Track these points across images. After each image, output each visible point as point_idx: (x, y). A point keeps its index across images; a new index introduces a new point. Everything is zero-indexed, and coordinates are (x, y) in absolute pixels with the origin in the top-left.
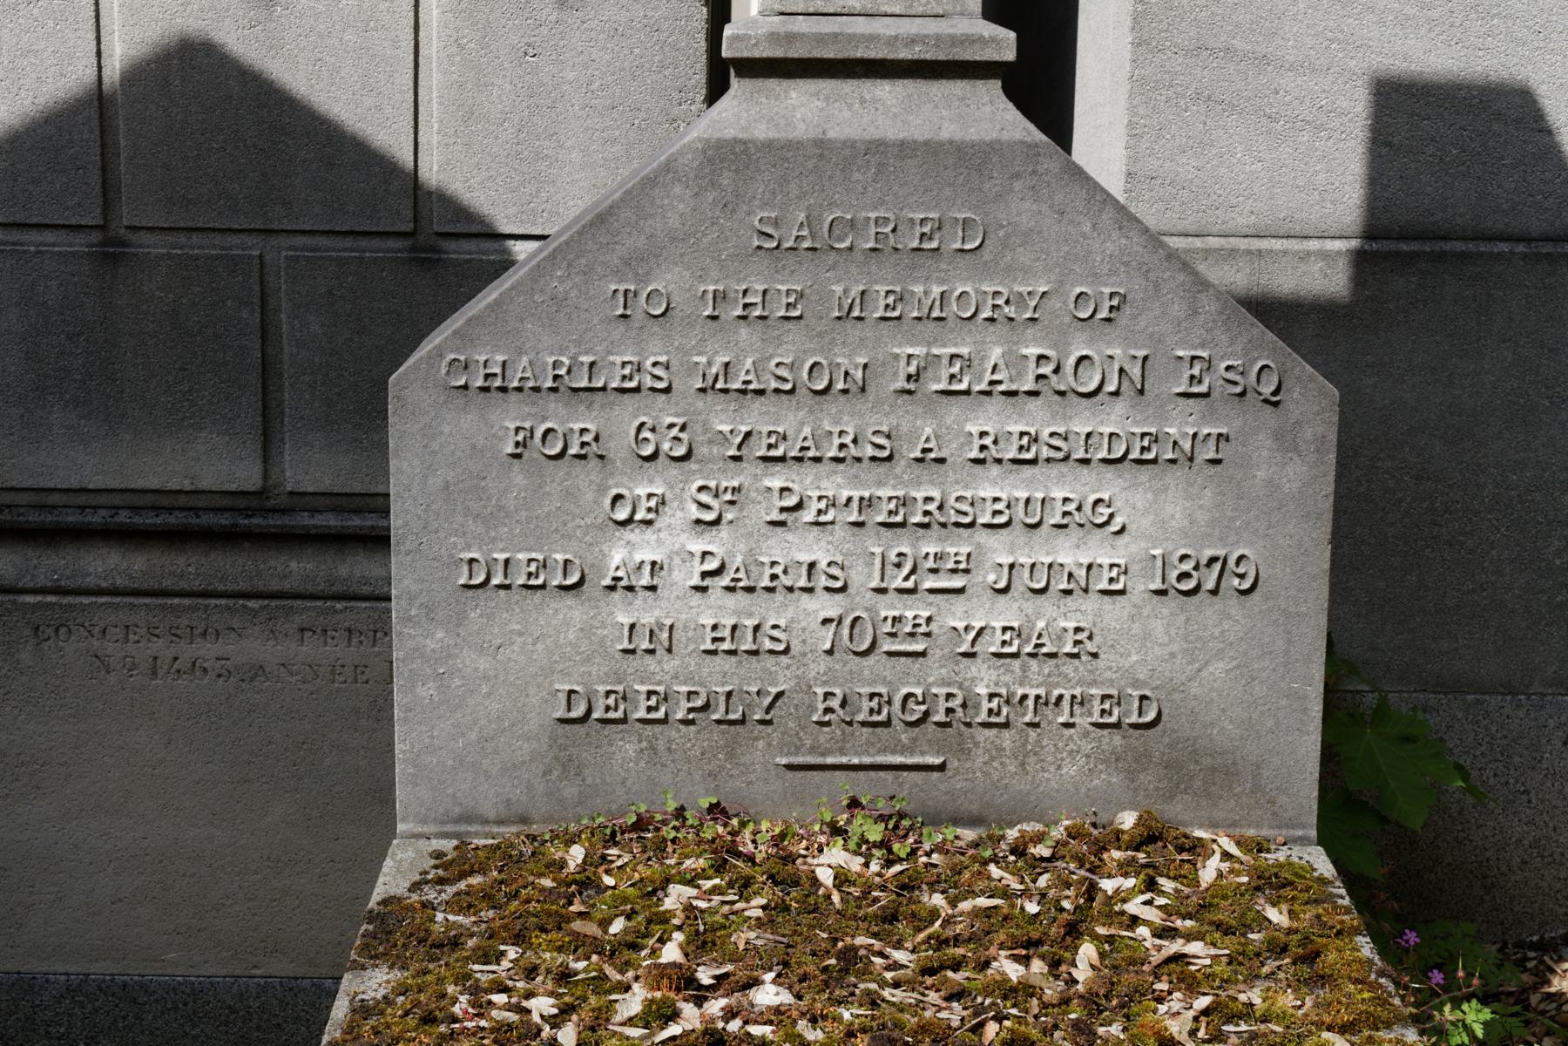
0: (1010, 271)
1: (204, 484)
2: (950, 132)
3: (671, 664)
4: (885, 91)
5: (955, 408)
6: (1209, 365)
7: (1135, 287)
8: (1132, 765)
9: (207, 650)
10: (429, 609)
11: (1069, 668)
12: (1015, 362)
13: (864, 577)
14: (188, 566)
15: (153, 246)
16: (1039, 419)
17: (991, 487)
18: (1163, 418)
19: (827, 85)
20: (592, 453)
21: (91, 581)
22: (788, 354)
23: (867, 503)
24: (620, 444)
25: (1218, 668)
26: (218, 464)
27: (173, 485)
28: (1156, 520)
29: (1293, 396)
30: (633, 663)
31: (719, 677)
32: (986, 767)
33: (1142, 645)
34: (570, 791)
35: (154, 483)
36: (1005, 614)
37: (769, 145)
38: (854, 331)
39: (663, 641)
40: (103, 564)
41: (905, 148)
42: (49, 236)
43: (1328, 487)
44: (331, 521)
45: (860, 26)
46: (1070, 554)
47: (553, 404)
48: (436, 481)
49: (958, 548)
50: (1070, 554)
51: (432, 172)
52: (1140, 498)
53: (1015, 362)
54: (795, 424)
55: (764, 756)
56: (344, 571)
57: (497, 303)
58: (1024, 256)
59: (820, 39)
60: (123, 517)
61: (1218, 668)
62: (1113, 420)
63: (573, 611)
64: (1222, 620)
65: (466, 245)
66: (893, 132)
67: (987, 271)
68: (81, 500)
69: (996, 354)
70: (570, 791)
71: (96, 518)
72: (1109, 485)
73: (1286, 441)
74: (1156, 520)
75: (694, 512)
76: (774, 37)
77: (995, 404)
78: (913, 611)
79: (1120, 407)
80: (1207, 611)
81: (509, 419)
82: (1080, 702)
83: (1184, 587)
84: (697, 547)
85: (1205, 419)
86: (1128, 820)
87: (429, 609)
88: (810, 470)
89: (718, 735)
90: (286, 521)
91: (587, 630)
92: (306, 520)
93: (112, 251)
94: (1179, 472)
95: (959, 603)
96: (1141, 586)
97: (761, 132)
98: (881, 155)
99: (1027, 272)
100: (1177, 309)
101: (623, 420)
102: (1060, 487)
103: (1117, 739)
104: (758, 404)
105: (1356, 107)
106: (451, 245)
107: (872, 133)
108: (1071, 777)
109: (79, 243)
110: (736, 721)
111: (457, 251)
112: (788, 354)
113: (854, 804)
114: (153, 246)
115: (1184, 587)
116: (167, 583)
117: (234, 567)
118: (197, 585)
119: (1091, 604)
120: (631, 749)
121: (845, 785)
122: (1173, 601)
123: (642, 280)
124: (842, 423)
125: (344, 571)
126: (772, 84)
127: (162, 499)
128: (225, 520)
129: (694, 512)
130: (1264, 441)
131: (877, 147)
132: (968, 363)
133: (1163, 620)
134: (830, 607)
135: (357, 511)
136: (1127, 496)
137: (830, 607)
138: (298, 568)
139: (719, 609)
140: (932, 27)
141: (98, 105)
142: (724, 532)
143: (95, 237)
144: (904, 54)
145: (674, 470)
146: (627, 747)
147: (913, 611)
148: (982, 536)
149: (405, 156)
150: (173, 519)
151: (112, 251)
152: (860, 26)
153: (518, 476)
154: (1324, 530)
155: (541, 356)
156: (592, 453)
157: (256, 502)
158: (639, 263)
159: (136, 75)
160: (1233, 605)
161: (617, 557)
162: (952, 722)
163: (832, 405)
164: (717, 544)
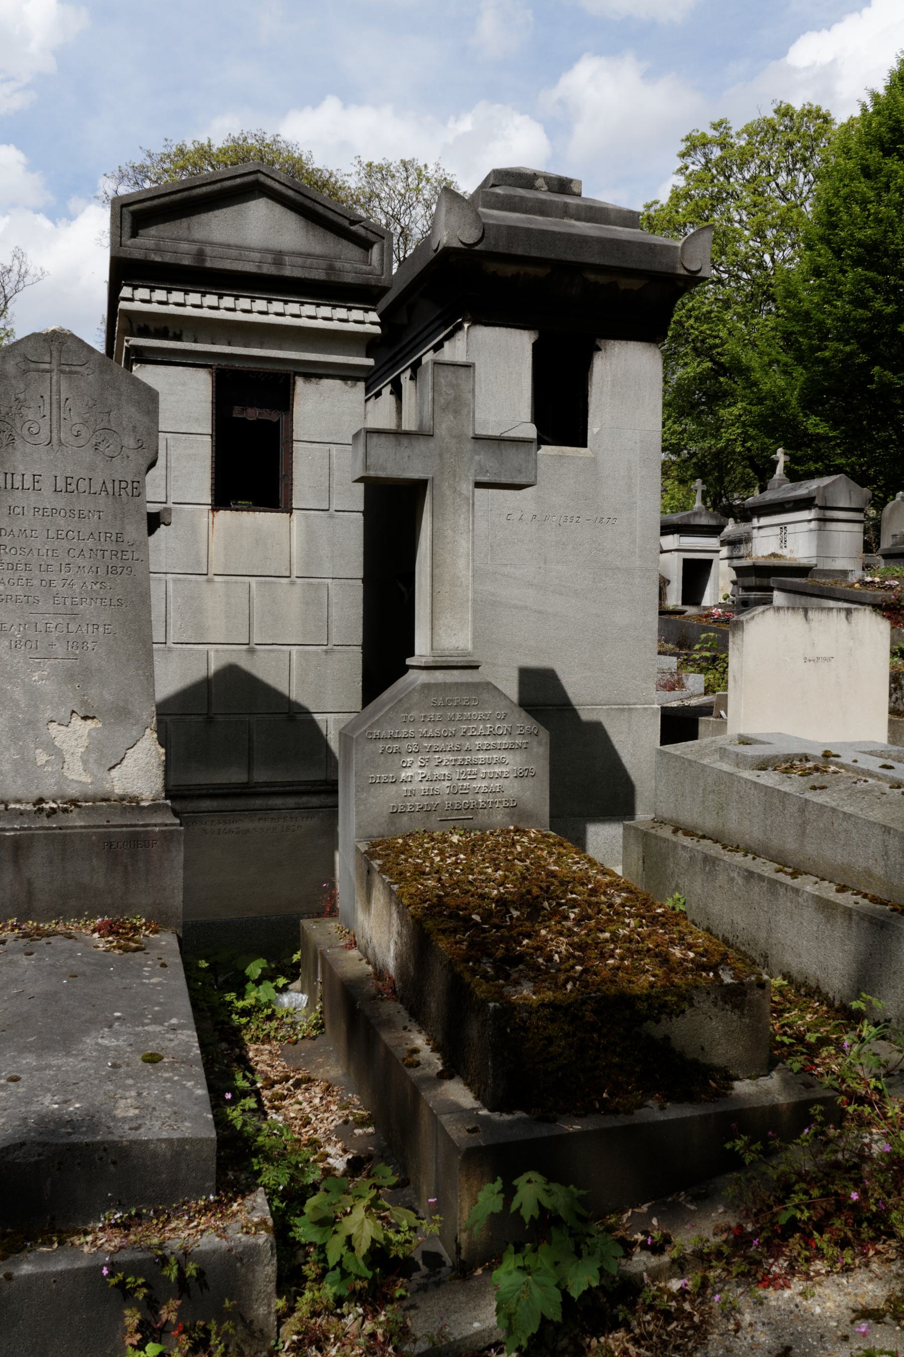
0: (484, 709)
1: (233, 781)
2: (470, 680)
3: (415, 798)
4: (455, 672)
5: (473, 739)
6: (524, 728)
7: (508, 711)
8: (511, 815)
9: (233, 826)
10: (363, 789)
11: (498, 795)
12: (485, 728)
13: (455, 777)
14: (229, 804)
15: (220, 718)
16: (490, 741)
17: (481, 756)
18: (515, 739)
19: (444, 671)
20: (398, 752)
21: (203, 809)
22: (439, 729)
23: (456, 760)
24: (403, 751)
25: (528, 793)
26: (236, 776)
27: (224, 782)
28: (513, 762)
29: (541, 733)
30: (406, 799)
31: (425, 801)
32: (481, 818)
33: (513, 789)
34: (393, 829)
35: (219, 782)
36: (484, 784)
37: (434, 684)
38: (453, 723)
39: (413, 793)
40: (206, 804)
41: (462, 684)
42: (193, 717)
43: (548, 753)
44: (267, 789)
45: (449, 659)
46: (497, 769)
47: (390, 741)
48: (364, 759)
49: (475, 770)
50: (497, 769)
51: (294, 697)
52: (511, 757)
53: (485, 728)
54: (440, 744)
55: (435, 818)
56: (270, 802)
57: (378, 720)
58: (487, 706)
59: (443, 662)
60: (211, 791)
61: (528, 793)
62: (505, 740)
63: (394, 788)
64: (529, 782)
65: (301, 715)
66: (459, 681)
67: (479, 709)
68: (198, 787)
69: (481, 727)
70: (393, 829)
71: (204, 792)
72: (504, 754)
73: (540, 743)
74: (513, 762)
75: (420, 764)
76: (433, 662)
77: (481, 738)
78: (466, 784)
79: (506, 737)
80: (526, 780)
81: (380, 745)
82: (501, 802)
83: (520, 776)
84: (420, 771)
85: (524, 739)
86: (512, 828)
87: (363, 789)
88: (444, 754)
89: (425, 814)
90: (252, 790)
91: (396, 792)
92: (259, 789)
93: (209, 720)
94: (518, 751)
95: (475, 782)
96: (512, 776)
97: (433, 681)
98: (458, 686)
99: (487, 709)
100: (517, 716)
101: (405, 744)
102: (495, 755)
103: (508, 810)
104: (433, 740)
105: (515, 674)
106: (298, 715)
107: (455, 681)
108: (499, 818)
109: (200, 718)
110: (428, 811)
111: (300, 717)
112: (439, 729)
113: (454, 828)
114: (220, 718)
115: (520, 776)
116: (223, 809)
117: (241, 803)
118: (231, 808)
119: (502, 780)
120: (406, 818)
121: (452, 823)
122: (519, 779)
123: (408, 713)
124: (451, 743)
125: (270, 802)
126: (432, 671)
127: (221, 786)
128: (239, 790)
129: (420, 764)
130: (535, 743)
131: (456, 684)
132: (476, 729)
133: (516, 783)
134: (447, 784)
135: (273, 787)
136: (507, 756)
137: (447, 784)
138: (258, 802)
139: (424, 786)
140: (464, 659)
141: (207, 683)
142: (426, 768)
143: (205, 716)
144: (459, 664)
145: (415, 755)
146: (405, 818)
147: (466, 784)
148: (480, 767)
149: (286, 692)
150: (225, 791)
151: (209, 720)
152: (449, 659)
153: (382, 758)
154: (548, 762)
155: (388, 731)
156: (398, 752)
157: (245, 785)
158: (408, 710)
159: (218, 674)
160: (530, 779)
161: (403, 775)
162: (474, 809)
163: (448, 739)
164: (424, 771)
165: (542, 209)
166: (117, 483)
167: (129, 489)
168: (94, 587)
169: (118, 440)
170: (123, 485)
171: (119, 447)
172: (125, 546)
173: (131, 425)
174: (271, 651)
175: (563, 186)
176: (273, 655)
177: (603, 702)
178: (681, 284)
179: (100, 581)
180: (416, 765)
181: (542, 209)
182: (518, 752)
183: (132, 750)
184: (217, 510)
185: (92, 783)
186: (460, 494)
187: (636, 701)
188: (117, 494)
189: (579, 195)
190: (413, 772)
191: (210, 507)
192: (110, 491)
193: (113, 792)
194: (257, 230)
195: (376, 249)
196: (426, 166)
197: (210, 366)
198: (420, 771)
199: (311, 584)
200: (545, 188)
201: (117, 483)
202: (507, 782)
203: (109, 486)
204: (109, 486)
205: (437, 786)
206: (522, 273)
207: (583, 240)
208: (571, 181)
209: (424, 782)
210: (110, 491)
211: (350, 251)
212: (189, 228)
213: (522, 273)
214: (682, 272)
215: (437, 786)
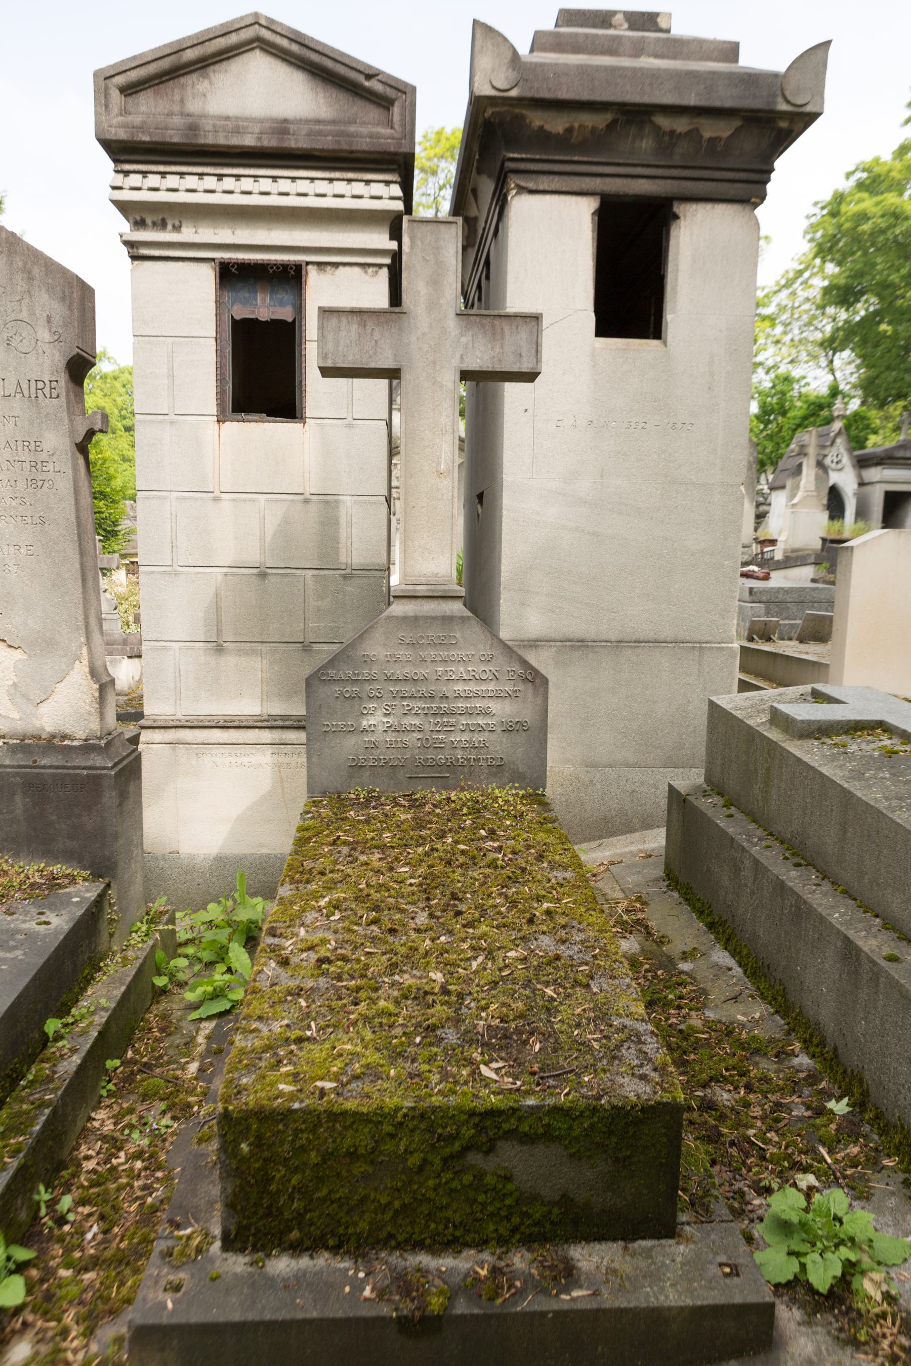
9: (245, 760)
13: (426, 727)
16: (472, 687)
25: (519, 751)
31: (391, 755)
36: (465, 737)
39: (375, 746)
46: (481, 721)
49: (452, 720)
50: (481, 721)
62: (492, 686)
79: (493, 683)
84: (385, 720)
95: (453, 734)
96: (499, 729)
119: (487, 734)
122: (506, 735)
133: (505, 738)
152: (439, 587)
161: (365, 723)
164: (390, 720)
165: (612, 47)
166: (33, 384)
167: (47, 391)
168: (13, 503)
169: (32, 332)
170: (40, 385)
171: (33, 343)
172: (43, 456)
173: (45, 315)
174: (283, 575)
175: (646, 21)
176: (286, 579)
177: (668, 639)
178: (783, 124)
179: (19, 495)
180: (380, 712)
181: (612, 47)
182: (508, 701)
183: (62, 684)
184: (224, 422)
185: (21, 719)
186: (441, 386)
187: (709, 638)
188: (33, 396)
189: (668, 31)
190: (375, 719)
191: (215, 418)
192: (26, 393)
193: (43, 729)
194: (258, 95)
195: (396, 110)
196: (808, 217)
197: (213, 260)
198: (385, 720)
199: (327, 502)
200: (626, 26)
201: (33, 384)
202: (493, 737)
203: (25, 386)
204: (25, 386)
205: (406, 738)
206: (576, 125)
207: (654, 75)
208: (657, 15)
209: (390, 733)
210: (26, 393)
211: (373, 113)
212: (182, 101)
213: (576, 125)
214: (783, 107)
215: (406, 738)
